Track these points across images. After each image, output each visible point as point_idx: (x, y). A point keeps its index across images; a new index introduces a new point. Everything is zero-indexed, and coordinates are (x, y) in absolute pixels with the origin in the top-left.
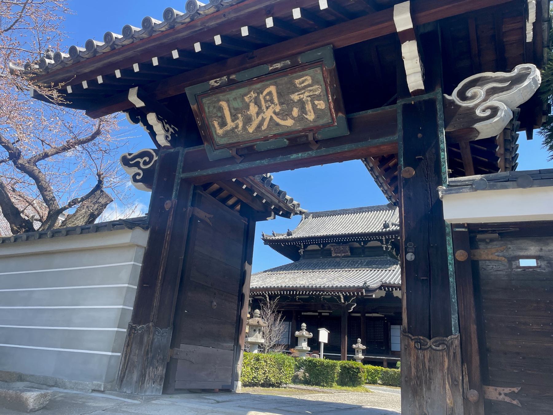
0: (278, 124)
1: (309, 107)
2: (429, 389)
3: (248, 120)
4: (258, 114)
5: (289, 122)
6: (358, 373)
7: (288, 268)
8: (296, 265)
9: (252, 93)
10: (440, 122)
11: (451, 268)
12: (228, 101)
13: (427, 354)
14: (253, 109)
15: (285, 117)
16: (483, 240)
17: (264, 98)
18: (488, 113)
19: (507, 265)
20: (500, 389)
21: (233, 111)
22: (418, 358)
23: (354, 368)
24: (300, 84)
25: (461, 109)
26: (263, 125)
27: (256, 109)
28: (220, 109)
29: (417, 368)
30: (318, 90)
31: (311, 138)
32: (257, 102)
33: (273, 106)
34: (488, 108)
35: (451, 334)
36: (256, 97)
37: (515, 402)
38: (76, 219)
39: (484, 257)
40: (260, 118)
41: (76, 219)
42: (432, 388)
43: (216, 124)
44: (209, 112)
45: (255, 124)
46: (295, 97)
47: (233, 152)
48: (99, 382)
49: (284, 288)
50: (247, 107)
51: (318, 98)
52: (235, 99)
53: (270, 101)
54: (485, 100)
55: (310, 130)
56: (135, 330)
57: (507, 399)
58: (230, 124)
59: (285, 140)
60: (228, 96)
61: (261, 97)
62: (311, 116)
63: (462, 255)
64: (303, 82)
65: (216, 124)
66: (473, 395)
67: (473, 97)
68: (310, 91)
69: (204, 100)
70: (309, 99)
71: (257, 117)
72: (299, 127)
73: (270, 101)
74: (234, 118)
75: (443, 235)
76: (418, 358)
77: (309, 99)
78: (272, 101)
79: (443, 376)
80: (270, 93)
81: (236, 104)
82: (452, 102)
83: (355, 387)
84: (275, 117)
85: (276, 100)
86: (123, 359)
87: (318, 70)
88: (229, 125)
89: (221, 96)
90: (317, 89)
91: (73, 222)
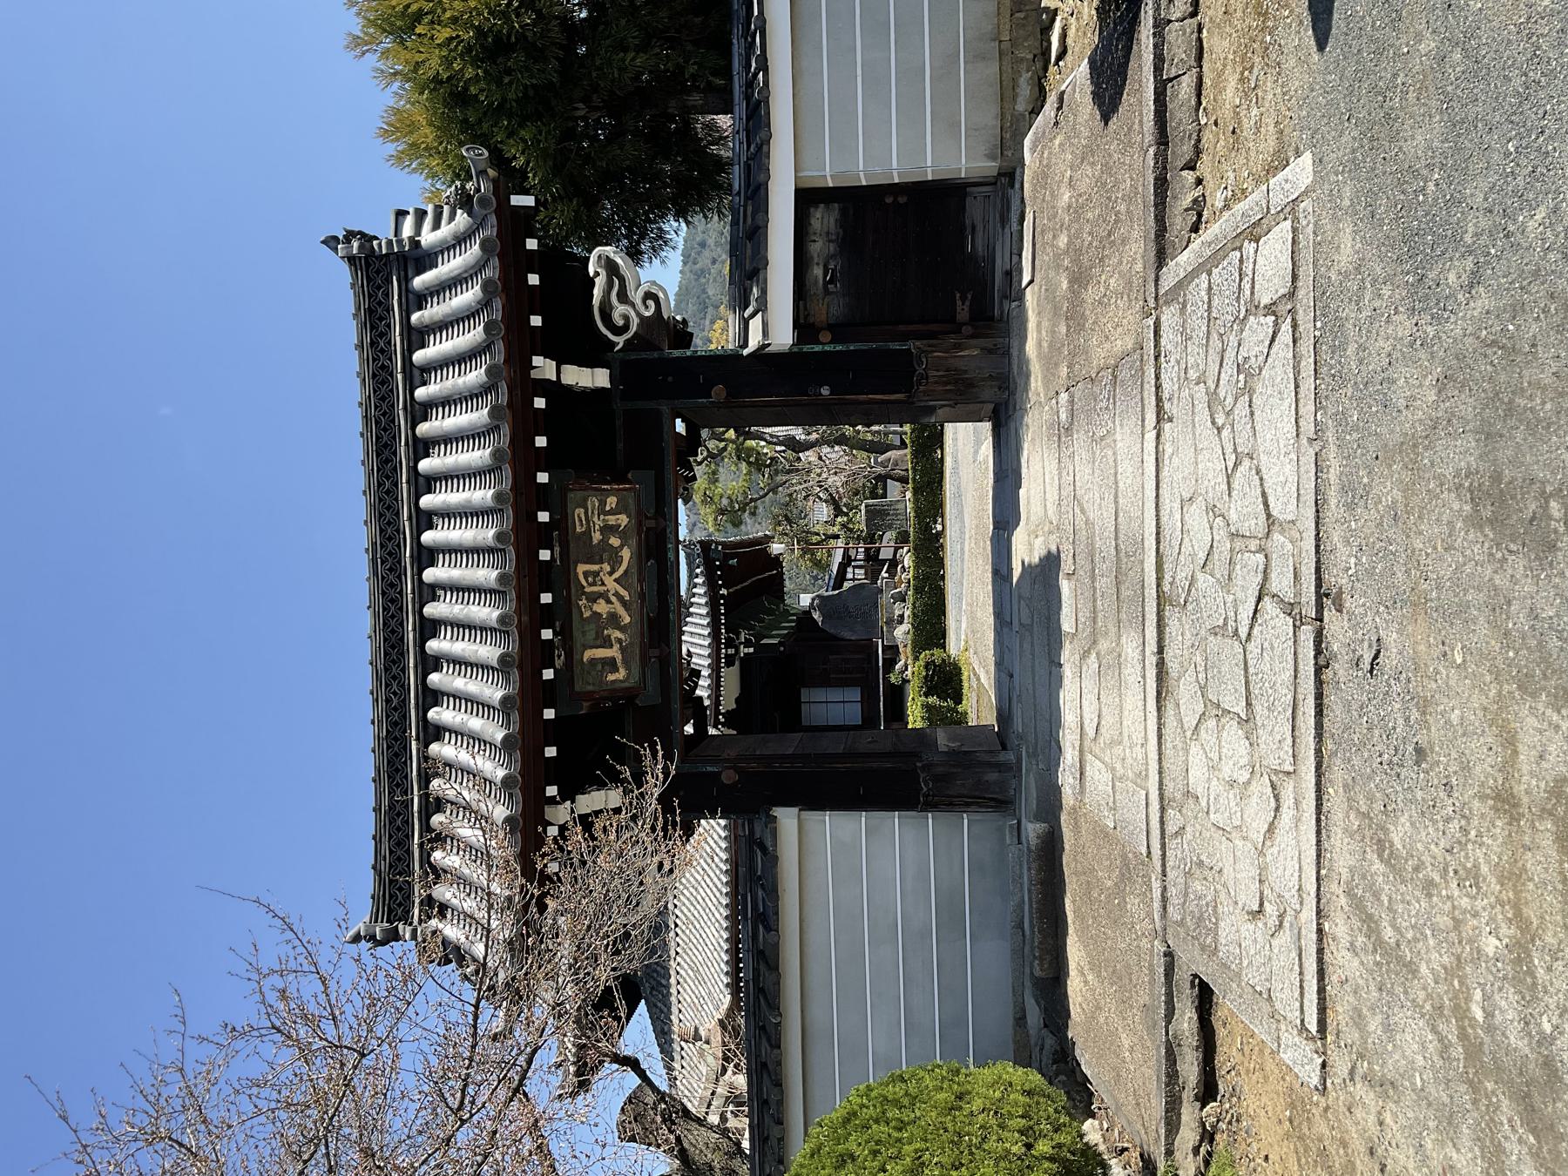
0: (626, 572)
1: (612, 520)
2: (966, 372)
3: (614, 619)
4: (609, 602)
5: (626, 554)
6: (935, 666)
7: (662, 1012)
8: (653, 988)
9: (581, 603)
10: (656, 355)
11: (839, 348)
12: (586, 647)
13: (932, 373)
14: (601, 607)
15: (619, 559)
16: (806, 317)
17: (590, 585)
18: (651, 303)
19: (832, 296)
20: (958, 309)
21: (598, 643)
22: (936, 383)
23: (927, 675)
24: (582, 525)
25: (640, 332)
26: (623, 597)
27: (602, 601)
28: (593, 661)
29: (946, 384)
30: (594, 502)
31: (652, 524)
32: (593, 598)
33: (601, 574)
34: (644, 302)
35: (909, 349)
36: (586, 599)
37: (969, 296)
38: (695, 1146)
39: (824, 317)
40: (613, 599)
41: (695, 1146)
42: (964, 368)
43: (611, 677)
44: (594, 684)
45: (621, 611)
46: (597, 537)
47: (655, 652)
48: (1007, 833)
49: (732, 979)
50: (597, 615)
51: (603, 503)
52: (584, 633)
53: (595, 577)
54: (633, 305)
55: (640, 524)
56: (929, 795)
57: (968, 303)
58: (613, 652)
59: (649, 564)
60: (578, 645)
61: (588, 589)
62: (623, 520)
63: (825, 336)
64: (581, 520)
65: (611, 677)
66: (967, 330)
67: (626, 318)
68: (593, 513)
69: (577, 688)
70: (602, 517)
71: (612, 603)
72: (634, 542)
73: (595, 577)
74: (607, 643)
75: (801, 355)
76: (936, 383)
77: (602, 517)
78: (596, 574)
79: (951, 357)
80: (586, 574)
81: (591, 635)
82: (627, 342)
83: (960, 669)
84: (616, 575)
85: (595, 567)
86: (973, 808)
87: (571, 495)
88: (616, 655)
89: (576, 657)
90: (593, 502)
91: (701, 1151)
